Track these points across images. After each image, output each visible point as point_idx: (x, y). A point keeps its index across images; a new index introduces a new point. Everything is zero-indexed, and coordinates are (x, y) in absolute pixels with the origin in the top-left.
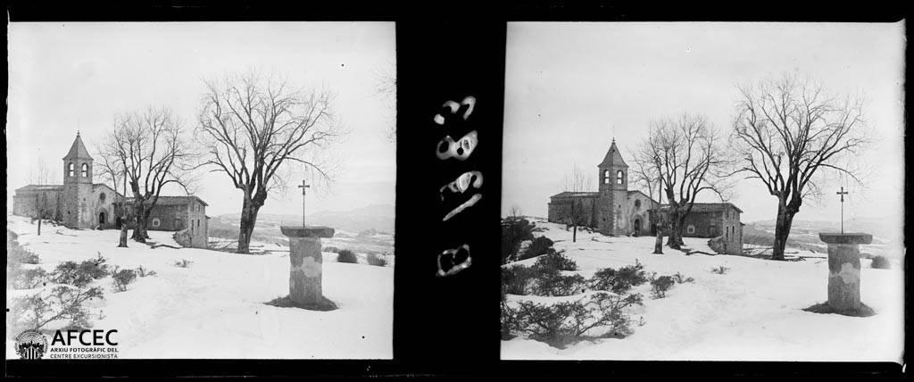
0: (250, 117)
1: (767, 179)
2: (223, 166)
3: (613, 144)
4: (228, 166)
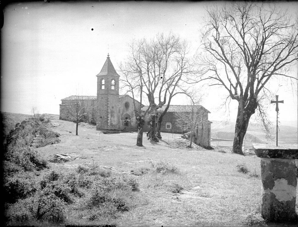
0: (244, 40)
1: (229, 87)
2: (221, 81)
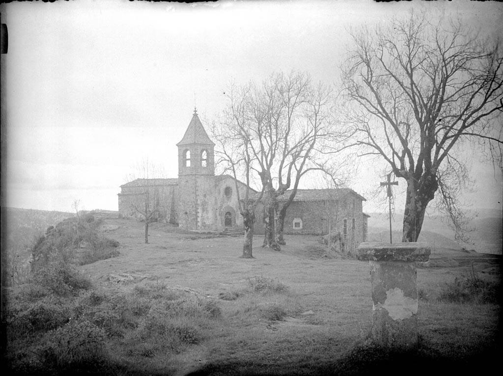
1: (390, 157)
2: (378, 148)
3: (195, 115)
4: (388, 151)
